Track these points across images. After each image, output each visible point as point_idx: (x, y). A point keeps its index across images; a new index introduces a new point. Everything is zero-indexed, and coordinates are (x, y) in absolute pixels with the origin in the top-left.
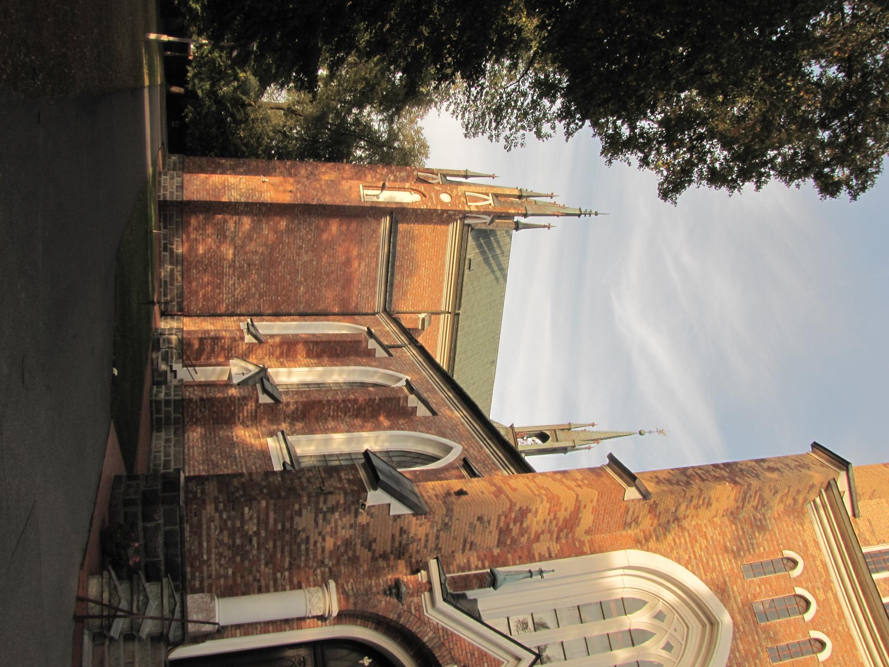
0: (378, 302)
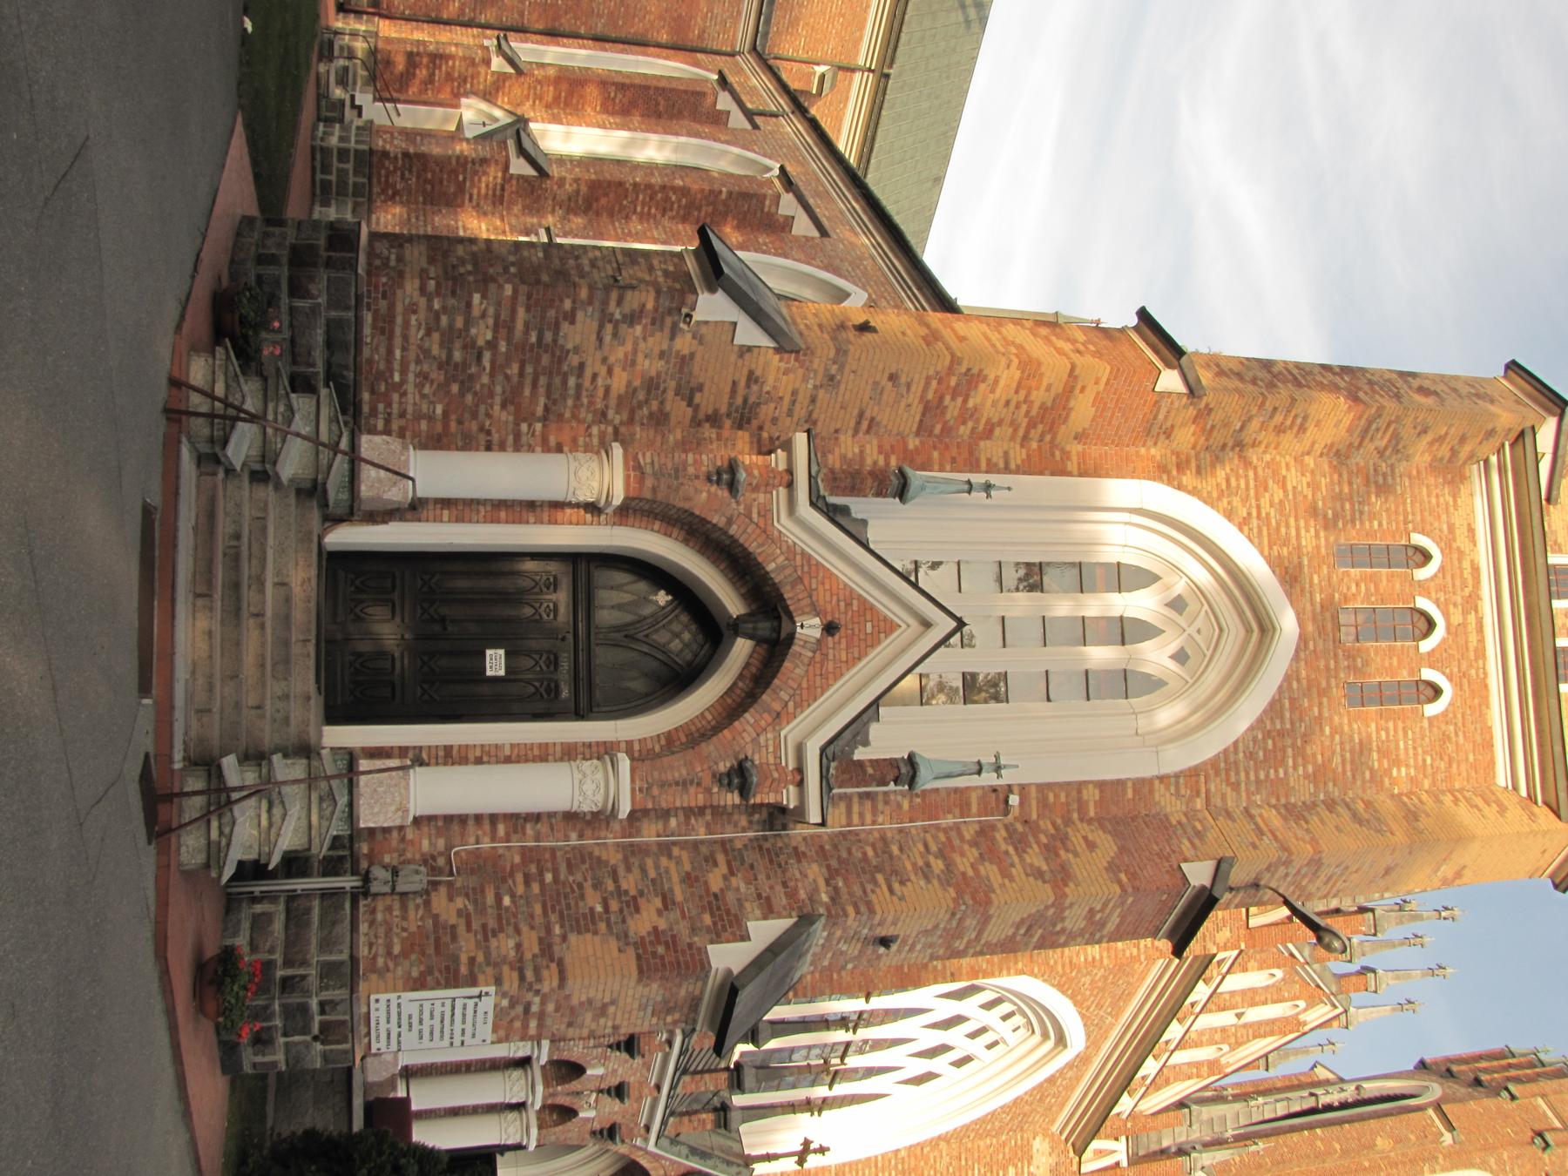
0: (742, 34)
